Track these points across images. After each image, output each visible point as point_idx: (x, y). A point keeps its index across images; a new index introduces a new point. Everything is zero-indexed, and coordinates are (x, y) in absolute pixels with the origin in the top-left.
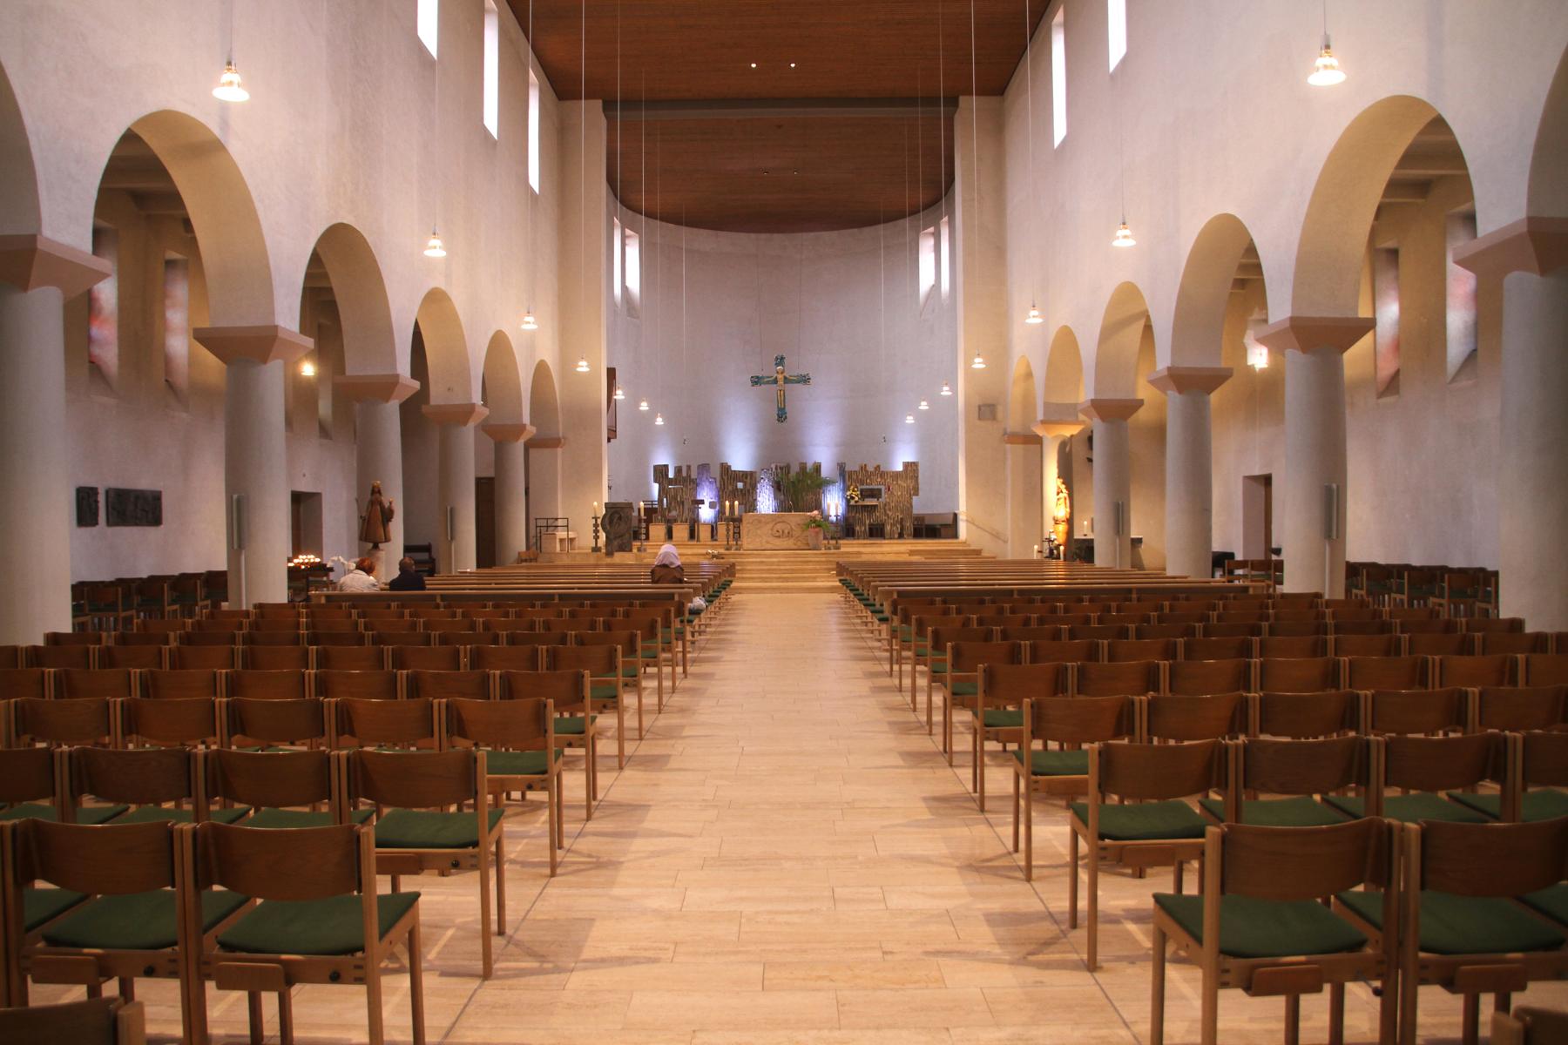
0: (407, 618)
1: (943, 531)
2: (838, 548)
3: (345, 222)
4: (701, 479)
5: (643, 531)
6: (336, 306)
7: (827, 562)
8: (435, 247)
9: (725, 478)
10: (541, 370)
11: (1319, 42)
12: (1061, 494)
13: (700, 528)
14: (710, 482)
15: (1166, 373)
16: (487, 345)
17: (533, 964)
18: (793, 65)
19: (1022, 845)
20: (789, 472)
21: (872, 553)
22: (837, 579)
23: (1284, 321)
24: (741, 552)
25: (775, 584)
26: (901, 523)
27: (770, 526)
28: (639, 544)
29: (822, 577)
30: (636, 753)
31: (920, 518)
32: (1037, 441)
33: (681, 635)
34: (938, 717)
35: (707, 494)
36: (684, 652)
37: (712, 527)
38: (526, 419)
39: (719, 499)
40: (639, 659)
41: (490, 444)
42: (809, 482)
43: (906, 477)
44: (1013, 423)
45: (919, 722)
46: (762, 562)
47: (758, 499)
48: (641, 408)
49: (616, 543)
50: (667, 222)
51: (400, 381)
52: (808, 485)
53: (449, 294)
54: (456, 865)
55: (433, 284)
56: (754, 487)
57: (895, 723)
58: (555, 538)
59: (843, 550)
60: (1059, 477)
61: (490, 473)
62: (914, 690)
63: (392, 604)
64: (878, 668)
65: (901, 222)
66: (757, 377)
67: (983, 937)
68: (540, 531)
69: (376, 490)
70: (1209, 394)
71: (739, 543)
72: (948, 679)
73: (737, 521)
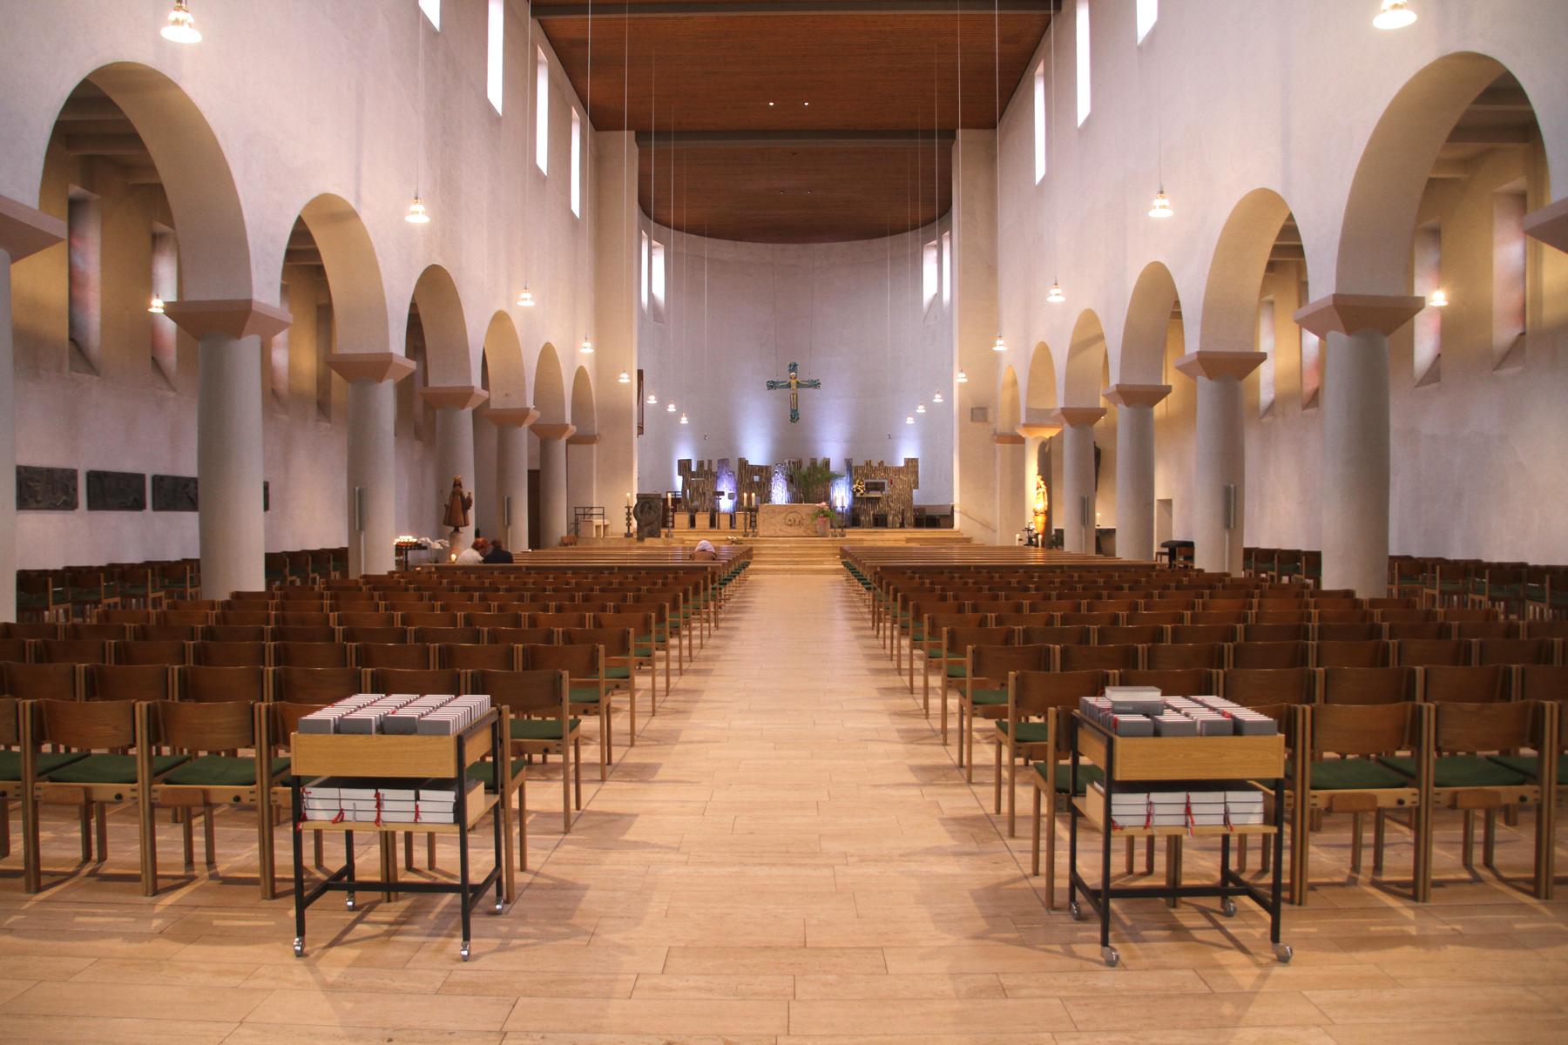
1: (942, 522)
2: (843, 535)
3: (436, 263)
4: (721, 472)
5: (671, 519)
6: (422, 328)
7: (833, 547)
8: (526, 299)
9: (744, 471)
10: (581, 375)
13: (721, 517)
14: (729, 476)
15: (1196, 357)
17: (655, 743)
18: (806, 104)
19: (1043, 868)
21: (873, 540)
23: (1192, 354)
25: (787, 567)
26: (903, 514)
27: (784, 515)
28: (666, 530)
30: (624, 761)
31: (921, 510)
32: (1019, 441)
33: (714, 598)
34: (953, 724)
35: (726, 486)
37: (731, 516)
38: (568, 420)
39: (737, 490)
40: (632, 658)
43: (908, 471)
44: (1002, 423)
45: (933, 730)
46: (776, 547)
47: (773, 491)
48: (669, 410)
49: (646, 530)
50: (691, 233)
52: (818, 479)
53: (510, 314)
54: (618, 687)
55: (497, 308)
56: (769, 480)
57: (908, 731)
58: (592, 525)
59: (847, 537)
61: (537, 466)
62: (884, 638)
63: (472, 576)
64: (866, 625)
65: (905, 234)
66: (773, 382)
68: (580, 517)
69: (457, 483)
70: (1152, 407)
72: (968, 684)
73: (753, 511)
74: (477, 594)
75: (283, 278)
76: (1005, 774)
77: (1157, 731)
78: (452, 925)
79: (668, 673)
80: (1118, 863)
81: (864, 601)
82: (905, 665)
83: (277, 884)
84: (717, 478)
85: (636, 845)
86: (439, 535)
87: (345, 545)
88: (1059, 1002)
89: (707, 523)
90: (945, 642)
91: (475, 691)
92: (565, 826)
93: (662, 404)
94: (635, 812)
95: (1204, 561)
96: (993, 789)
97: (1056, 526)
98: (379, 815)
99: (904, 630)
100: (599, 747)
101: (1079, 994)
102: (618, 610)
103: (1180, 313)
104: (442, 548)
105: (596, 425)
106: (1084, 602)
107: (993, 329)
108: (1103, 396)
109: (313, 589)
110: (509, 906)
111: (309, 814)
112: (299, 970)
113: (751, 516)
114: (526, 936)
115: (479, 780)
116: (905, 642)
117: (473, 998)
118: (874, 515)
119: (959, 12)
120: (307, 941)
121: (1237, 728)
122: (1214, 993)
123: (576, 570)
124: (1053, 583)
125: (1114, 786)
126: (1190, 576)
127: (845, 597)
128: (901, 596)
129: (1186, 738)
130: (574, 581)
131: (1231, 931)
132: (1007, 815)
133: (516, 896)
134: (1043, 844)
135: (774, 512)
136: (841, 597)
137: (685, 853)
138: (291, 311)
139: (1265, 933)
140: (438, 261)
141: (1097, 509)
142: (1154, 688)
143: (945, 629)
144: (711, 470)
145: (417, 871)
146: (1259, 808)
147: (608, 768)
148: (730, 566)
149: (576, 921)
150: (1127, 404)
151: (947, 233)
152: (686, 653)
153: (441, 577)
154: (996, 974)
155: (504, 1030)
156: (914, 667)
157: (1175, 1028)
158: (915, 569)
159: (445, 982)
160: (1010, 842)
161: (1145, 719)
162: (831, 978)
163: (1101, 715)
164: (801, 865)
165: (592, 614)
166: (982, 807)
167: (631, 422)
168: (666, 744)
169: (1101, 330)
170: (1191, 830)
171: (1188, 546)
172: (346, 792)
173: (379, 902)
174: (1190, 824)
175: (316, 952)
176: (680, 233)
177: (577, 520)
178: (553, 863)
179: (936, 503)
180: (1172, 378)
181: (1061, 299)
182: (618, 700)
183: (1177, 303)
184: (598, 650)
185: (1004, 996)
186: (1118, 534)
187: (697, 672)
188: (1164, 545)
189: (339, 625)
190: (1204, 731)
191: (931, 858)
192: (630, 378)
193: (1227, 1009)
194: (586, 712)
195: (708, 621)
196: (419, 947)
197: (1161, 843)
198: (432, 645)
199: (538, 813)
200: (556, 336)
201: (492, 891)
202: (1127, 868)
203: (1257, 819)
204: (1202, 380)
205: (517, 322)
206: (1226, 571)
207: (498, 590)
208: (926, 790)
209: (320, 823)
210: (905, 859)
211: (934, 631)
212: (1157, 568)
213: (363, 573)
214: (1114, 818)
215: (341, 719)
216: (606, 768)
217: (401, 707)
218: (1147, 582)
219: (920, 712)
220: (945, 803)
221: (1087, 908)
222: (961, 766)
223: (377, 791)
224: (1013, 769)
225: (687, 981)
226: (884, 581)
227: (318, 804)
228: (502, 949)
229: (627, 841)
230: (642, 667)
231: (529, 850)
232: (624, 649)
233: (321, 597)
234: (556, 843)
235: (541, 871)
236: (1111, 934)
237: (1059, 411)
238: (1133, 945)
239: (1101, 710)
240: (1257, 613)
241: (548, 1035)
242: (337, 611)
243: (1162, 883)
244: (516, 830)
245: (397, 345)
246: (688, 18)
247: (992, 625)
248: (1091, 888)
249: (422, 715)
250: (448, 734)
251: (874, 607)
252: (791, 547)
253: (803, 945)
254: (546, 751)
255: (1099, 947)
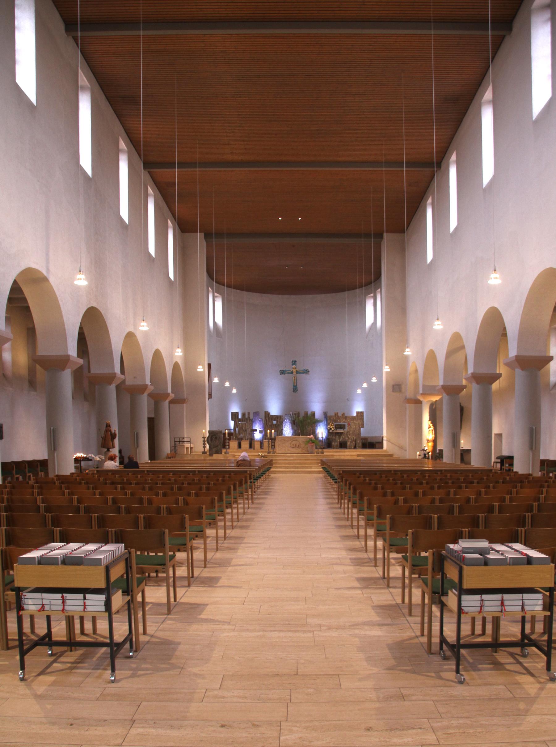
0: (66, 495)
1: (377, 445)
2: (323, 453)
3: (93, 306)
4: (255, 419)
5: (227, 444)
9: (267, 418)
10: (176, 366)
11: (493, 268)
12: (430, 428)
14: (260, 421)
16: (152, 356)
17: (218, 566)
20: (299, 416)
21: (339, 456)
22: (321, 467)
23: (513, 357)
24: (275, 454)
25: (292, 470)
26: (355, 441)
27: (290, 442)
28: (225, 450)
29: (314, 466)
31: (365, 439)
32: (419, 402)
33: (251, 487)
34: (380, 555)
35: (258, 427)
36: (252, 495)
37: (261, 442)
38: (170, 391)
40: (205, 521)
41: (152, 402)
42: (309, 421)
44: (409, 393)
45: (369, 558)
50: (237, 289)
51: (117, 376)
54: (197, 536)
57: (355, 559)
58: (184, 447)
59: (325, 454)
60: (429, 420)
61: (153, 416)
63: (117, 475)
64: (334, 501)
66: (283, 371)
67: (348, 561)
68: (177, 443)
69: (108, 425)
71: (274, 450)
73: (273, 440)
74: (119, 486)
75: (6, 313)
76: (407, 581)
77: (486, 563)
78: (106, 663)
79: (225, 528)
80: (466, 629)
81: (334, 488)
82: (355, 523)
83: (10, 642)
84: (253, 422)
85: (207, 621)
86: (99, 453)
87: (46, 458)
88: (432, 702)
89: (248, 446)
90: (375, 512)
91: (117, 542)
92: (168, 611)
93: (222, 382)
94: (206, 603)
95: (519, 467)
96: (400, 590)
97: (439, 448)
98: (64, 607)
99: (354, 505)
100: (186, 568)
101: (443, 699)
102: (197, 495)
103: (506, 334)
104: (100, 460)
105: (185, 393)
106: (452, 490)
107: (404, 343)
108: (465, 379)
109: (28, 483)
110: (137, 653)
111: (25, 607)
112: (22, 688)
113: (272, 443)
114: (146, 669)
115: (118, 588)
116: (355, 511)
117: (117, 702)
118: (340, 442)
119: (384, 169)
120: (26, 672)
121: (529, 561)
122: (515, 697)
123: (175, 473)
124: (436, 480)
125: (462, 592)
126: (510, 475)
127: (324, 486)
128: (353, 487)
129: (502, 567)
130: (173, 478)
131: (525, 665)
132: (407, 604)
133: (141, 649)
134: (426, 619)
135: (284, 440)
136: (322, 486)
137: (233, 625)
138: (12, 333)
139: (543, 666)
140: (94, 305)
141: (461, 439)
142: (485, 540)
143: (375, 506)
144: (249, 417)
145: (87, 635)
146: (541, 602)
147: (192, 579)
148: (260, 470)
149: (173, 661)
150: (478, 383)
151: (379, 290)
152: (235, 517)
153: (99, 476)
154: (399, 688)
155: (134, 719)
156: (360, 524)
157: (493, 716)
158: (361, 472)
159: (101, 694)
160: (409, 618)
161: (479, 557)
162: (310, 691)
163: (456, 554)
164: (296, 631)
165: (182, 497)
166: (395, 600)
167: (205, 392)
168: (224, 566)
169: (463, 343)
170: (504, 613)
171: (510, 459)
172: (45, 595)
173: (66, 651)
174: (503, 611)
175: (31, 678)
176: (230, 289)
177: (175, 444)
178: (161, 630)
179: (374, 436)
180: (502, 369)
181: (441, 327)
182: (198, 543)
183: (505, 329)
184: (185, 518)
185: (403, 699)
186: (472, 452)
187: (242, 527)
188: (498, 458)
189: (42, 504)
190: (511, 563)
191: (366, 627)
192: (204, 368)
193: (522, 706)
194: (179, 550)
195: (248, 499)
196: (88, 676)
197: (489, 619)
198: (94, 515)
199: (153, 603)
200: (162, 345)
201: (127, 645)
202: (471, 632)
203: (539, 608)
204: (518, 371)
205: (140, 338)
206: (531, 473)
207: (131, 484)
208: (364, 591)
209: (31, 611)
210: (352, 627)
211: (370, 507)
212: (493, 471)
213: (57, 474)
214: (463, 608)
215: (41, 557)
216: (190, 580)
217: (75, 550)
218: (487, 479)
219: (363, 549)
220: (374, 598)
221: (448, 653)
222: (384, 578)
223: (62, 595)
224: (411, 580)
225: (233, 693)
226: (344, 479)
227: (30, 602)
228: (133, 676)
229: (202, 619)
230: (160, 575)
231: (148, 624)
232: (200, 516)
233: (33, 487)
234: (163, 619)
235: (154, 635)
236: (461, 667)
237: (440, 387)
238: (473, 673)
239: (456, 551)
240: (545, 496)
241: (157, 722)
242: (42, 495)
243: (489, 639)
244: (140, 614)
245: (72, 350)
246: (232, 171)
247: (401, 503)
248: (451, 643)
249: (86, 554)
250: (101, 565)
251: (339, 491)
252: (294, 459)
253: (296, 673)
254: (157, 572)
255: (455, 673)
